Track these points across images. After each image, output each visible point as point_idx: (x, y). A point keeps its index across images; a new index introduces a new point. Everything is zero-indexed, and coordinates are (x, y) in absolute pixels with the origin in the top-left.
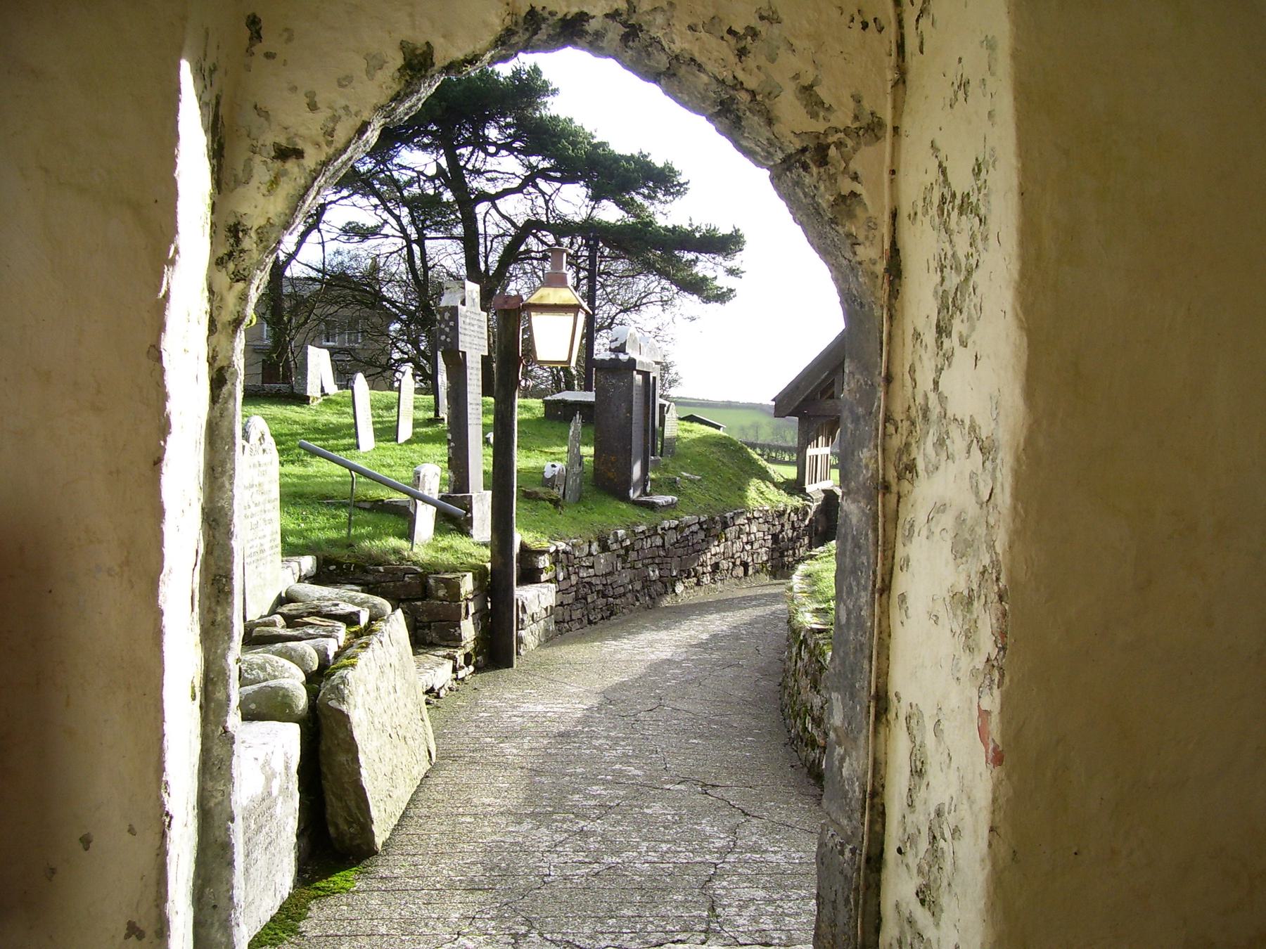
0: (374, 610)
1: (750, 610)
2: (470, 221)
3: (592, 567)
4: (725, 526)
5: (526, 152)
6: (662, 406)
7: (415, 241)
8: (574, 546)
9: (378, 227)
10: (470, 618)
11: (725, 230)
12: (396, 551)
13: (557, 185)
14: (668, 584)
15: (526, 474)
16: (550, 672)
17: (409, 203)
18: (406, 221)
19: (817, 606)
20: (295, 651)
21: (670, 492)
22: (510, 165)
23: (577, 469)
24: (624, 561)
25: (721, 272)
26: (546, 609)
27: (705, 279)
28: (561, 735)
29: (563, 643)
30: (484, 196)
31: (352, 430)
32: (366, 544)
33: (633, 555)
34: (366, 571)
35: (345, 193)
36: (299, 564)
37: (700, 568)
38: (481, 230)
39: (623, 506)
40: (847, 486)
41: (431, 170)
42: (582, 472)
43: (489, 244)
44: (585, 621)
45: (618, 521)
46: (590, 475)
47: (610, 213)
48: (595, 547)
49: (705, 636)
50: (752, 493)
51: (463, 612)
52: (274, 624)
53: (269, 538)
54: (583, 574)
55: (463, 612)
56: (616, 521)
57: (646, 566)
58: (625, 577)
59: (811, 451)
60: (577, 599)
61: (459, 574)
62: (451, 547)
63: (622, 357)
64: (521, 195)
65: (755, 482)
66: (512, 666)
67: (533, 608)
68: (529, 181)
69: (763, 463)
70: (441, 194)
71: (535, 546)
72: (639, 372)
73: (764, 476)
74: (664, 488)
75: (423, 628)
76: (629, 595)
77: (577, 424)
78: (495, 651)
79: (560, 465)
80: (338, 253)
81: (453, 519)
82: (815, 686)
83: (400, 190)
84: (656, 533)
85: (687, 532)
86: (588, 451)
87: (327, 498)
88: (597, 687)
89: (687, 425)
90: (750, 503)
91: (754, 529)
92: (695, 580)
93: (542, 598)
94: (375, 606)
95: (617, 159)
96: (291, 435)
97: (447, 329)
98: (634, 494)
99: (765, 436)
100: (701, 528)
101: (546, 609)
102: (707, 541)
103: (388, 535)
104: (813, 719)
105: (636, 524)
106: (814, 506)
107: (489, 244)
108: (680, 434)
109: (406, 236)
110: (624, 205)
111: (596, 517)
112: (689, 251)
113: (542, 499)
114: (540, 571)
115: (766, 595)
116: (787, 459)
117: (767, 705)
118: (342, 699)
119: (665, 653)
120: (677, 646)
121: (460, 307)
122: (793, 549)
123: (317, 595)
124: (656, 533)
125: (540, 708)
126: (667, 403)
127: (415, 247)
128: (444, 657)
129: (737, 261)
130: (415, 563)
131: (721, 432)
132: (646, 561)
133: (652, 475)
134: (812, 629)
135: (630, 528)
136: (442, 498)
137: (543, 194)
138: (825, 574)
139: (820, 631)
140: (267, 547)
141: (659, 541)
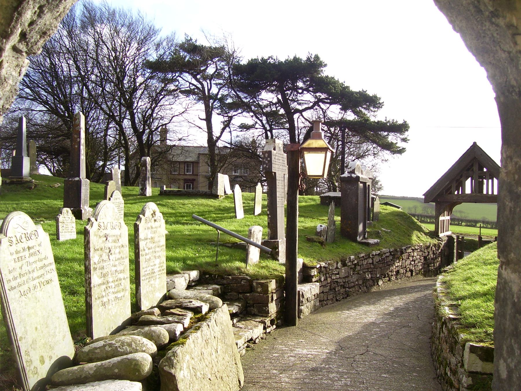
0: (212, 304)
1: (414, 294)
2: (291, 121)
3: (338, 274)
4: (402, 253)
5: (315, 92)
6: (373, 198)
7: (268, 130)
8: (329, 264)
9: (253, 125)
10: (274, 302)
11: (400, 122)
12: (238, 269)
13: (328, 105)
14: (375, 281)
15: (305, 230)
16: (313, 328)
17: (267, 115)
18: (264, 122)
19: (451, 302)
20: (154, 332)
21: (376, 238)
22: (308, 97)
23: (332, 227)
24: (354, 271)
25: (399, 140)
26: (315, 295)
27: (392, 143)
28: (314, 370)
29: (322, 311)
30: (297, 111)
31: (234, 210)
32: (224, 265)
33: (358, 268)
34: (223, 278)
35: (240, 111)
36: (189, 275)
37: (390, 273)
38: (296, 125)
39: (354, 244)
40: (506, 257)
41: (275, 100)
42: (335, 229)
43: (299, 131)
44: (334, 300)
45: (351, 252)
46: (339, 230)
47: (350, 116)
48: (339, 264)
49: (392, 309)
50: (414, 238)
51: (270, 299)
52: (152, 314)
53: (157, 266)
54: (334, 277)
55: (270, 299)
56: (350, 252)
57: (365, 273)
58: (354, 278)
59: (441, 218)
60: (330, 289)
61: (268, 280)
62: (267, 266)
63: (353, 175)
64: (312, 110)
65: (416, 232)
66: (295, 325)
67: (308, 295)
68: (316, 103)
69: (419, 223)
70: (279, 111)
71: (310, 264)
72: (361, 182)
73: (420, 229)
74: (374, 236)
75: (249, 307)
76: (356, 287)
77: (332, 207)
78: (287, 317)
79: (324, 226)
80: (237, 136)
81: (269, 251)
82: (452, 350)
83: (262, 109)
84: (369, 257)
85: (384, 256)
86: (338, 219)
87: (211, 241)
88: (336, 338)
89: (384, 207)
90: (413, 242)
91: (415, 254)
92: (388, 278)
93: (312, 290)
94: (213, 302)
95: (352, 93)
96: (209, 212)
97: (267, 162)
98: (359, 239)
99: (419, 211)
100: (391, 254)
101: (315, 295)
102: (393, 260)
103: (236, 260)
104: (451, 369)
105: (360, 253)
106: (443, 243)
107: (299, 131)
108: (381, 210)
109: (265, 128)
110: (355, 113)
111: (341, 250)
112: (385, 132)
113: (315, 241)
114: (312, 277)
115: (421, 286)
116: (429, 221)
117: (423, 351)
118: (172, 366)
119: (371, 318)
120: (378, 314)
121: (273, 151)
122: (434, 263)
123: (184, 295)
124: (369, 257)
125: (305, 351)
126: (375, 197)
127: (269, 133)
128: (259, 322)
129: (406, 134)
130: (247, 275)
131: (400, 210)
132: (365, 271)
133: (367, 230)
134: (450, 318)
135: (357, 255)
136: (263, 243)
137: (322, 109)
138: (453, 282)
139: (454, 319)
140: (156, 270)
141: (370, 261)
